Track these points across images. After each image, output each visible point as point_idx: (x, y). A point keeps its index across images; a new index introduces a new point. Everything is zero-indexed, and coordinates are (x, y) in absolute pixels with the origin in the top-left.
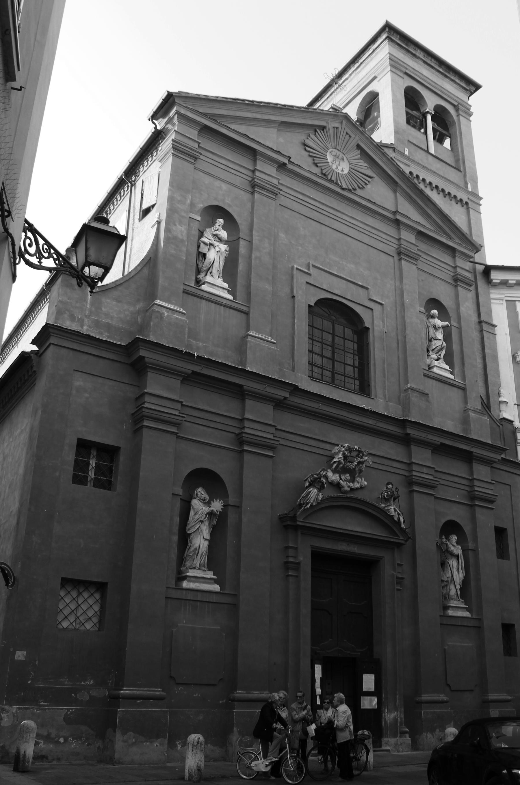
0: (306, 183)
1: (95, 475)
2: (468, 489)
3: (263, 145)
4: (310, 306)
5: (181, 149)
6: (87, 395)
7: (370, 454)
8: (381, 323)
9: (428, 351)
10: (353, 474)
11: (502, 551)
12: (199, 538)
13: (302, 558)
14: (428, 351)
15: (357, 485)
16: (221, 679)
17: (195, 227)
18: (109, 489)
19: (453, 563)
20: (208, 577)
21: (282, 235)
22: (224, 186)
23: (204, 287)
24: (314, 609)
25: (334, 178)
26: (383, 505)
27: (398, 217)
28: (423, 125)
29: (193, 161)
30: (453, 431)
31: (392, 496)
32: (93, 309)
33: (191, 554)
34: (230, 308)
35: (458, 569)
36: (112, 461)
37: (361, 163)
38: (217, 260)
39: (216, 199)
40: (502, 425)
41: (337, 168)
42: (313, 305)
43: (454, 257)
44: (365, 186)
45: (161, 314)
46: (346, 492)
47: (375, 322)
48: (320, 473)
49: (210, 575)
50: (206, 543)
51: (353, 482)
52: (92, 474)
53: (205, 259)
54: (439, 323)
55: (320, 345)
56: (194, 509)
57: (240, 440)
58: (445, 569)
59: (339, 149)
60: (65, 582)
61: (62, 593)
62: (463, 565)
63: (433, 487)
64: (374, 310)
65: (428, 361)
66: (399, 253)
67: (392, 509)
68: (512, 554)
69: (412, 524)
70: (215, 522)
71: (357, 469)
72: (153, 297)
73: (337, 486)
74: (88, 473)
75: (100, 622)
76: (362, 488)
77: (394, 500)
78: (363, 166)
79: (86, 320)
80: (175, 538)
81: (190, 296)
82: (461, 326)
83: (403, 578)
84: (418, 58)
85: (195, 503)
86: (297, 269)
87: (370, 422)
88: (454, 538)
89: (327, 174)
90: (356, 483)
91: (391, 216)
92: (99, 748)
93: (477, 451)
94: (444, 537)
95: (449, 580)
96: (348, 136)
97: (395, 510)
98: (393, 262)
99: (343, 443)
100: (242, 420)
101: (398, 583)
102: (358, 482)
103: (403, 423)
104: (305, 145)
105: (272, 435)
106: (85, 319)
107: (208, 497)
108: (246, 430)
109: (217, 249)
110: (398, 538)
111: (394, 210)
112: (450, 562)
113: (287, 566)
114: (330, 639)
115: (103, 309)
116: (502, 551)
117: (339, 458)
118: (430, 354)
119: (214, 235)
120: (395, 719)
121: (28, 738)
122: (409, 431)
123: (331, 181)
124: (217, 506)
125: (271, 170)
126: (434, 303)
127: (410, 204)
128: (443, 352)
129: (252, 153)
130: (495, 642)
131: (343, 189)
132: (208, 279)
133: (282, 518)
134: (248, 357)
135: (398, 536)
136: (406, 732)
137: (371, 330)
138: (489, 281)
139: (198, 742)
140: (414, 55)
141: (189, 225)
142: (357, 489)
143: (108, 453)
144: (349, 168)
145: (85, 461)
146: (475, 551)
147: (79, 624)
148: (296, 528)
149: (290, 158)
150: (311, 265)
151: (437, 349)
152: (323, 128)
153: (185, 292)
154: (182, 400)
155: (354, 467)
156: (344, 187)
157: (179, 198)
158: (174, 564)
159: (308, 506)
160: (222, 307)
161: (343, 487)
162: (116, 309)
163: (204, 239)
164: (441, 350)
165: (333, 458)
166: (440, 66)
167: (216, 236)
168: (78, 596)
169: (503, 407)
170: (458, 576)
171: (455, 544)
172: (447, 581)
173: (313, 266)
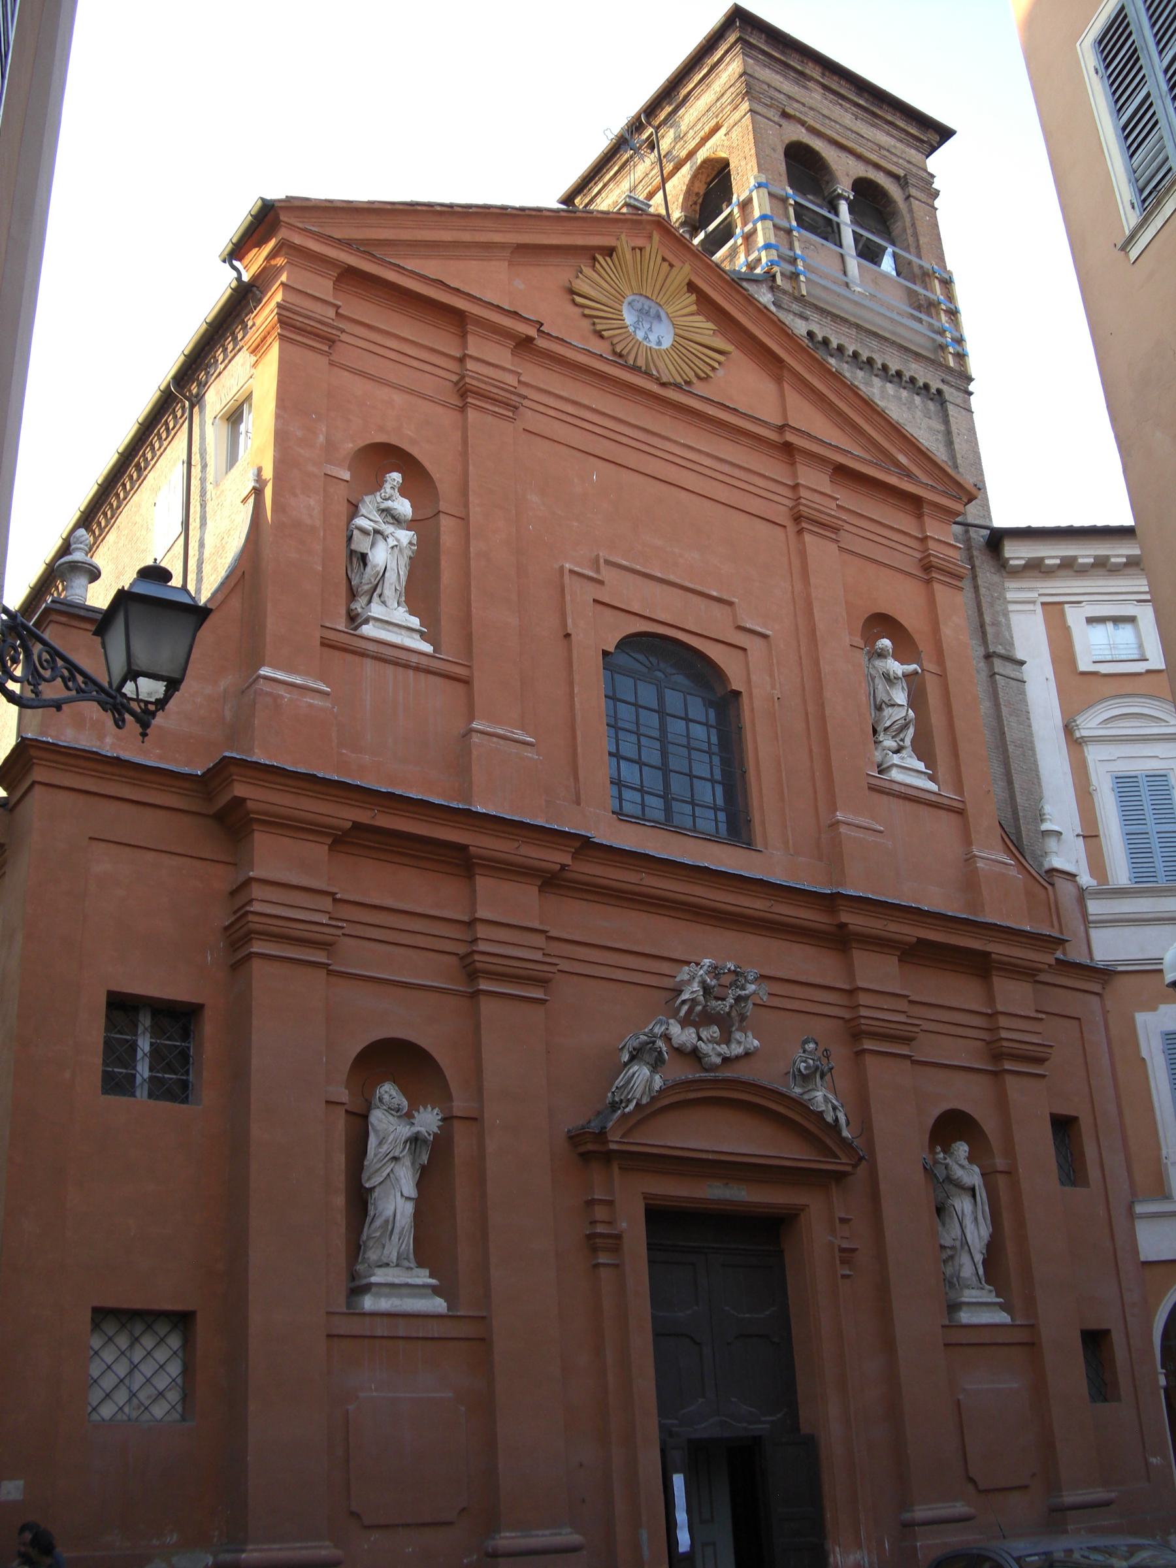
1: (151, 1070)
3: (480, 300)
4: (605, 654)
8: (768, 678)
9: (875, 732)
10: (726, 1025)
11: (1072, 1169)
12: (392, 1197)
13: (624, 1225)
14: (875, 732)
15: (736, 1050)
16: (463, 1509)
17: (340, 494)
18: (185, 1100)
20: (419, 1281)
21: (534, 498)
22: (398, 398)
24: (659, 1334)
25: (641, 362)
26: (798, 1090)
27: (790, 437)
28: (830, 231)
31: (817, 1068)
35: (976, 1219)
36: (186, 1035)
38: (392, 565)
40: (1052, 885)
41: (646, 338)
43: (920, 516)
44: (711, 374)
45: (276, 698)
46: (713, 1068)
49: (422, 1277)
50: (409, 1208)
51: (728, 1042)
52: (143, 1070)
53: (365, 565)
54: (895, 667)
55: (634, 738)
56: (376, 1131)
58: (947, 1220)
61: (96, 1342)
63: (907, 1040)
64: (749, 652)
65: (878, 756)
66: (798, 518)
67: (820, 1097)
68: (1094, 1173)
69: (866, 1127)
70: (425, 1159)
71: (734, 1014)
73: (695, 1055)
74: (134, 1068)
75: (185, 1399)
77: (822, 1076)
78: (704, 328)
80: (340, 1201)
82: (944, 670)
83: (854, 1250)
84: (811, 79)
85: (379, 1119)
86: (571, 571)
88: (962, 1149)
89: (624, 352)
90: (733, 1046)
91: (772, 435)
93: (999, 949)
94: (939, 1149)
95: (958, 1244)
96: (666, 264)
99: (702, 959)
100: (471, 923)
101: (843, 1262)
102: (739, 1043)
103: (831, 901)
104: (572, 292)
105: (541, 953)
109: (391, 542)
110: (835, 1160)
114: (701, 1400)
116: (1072, 1169)
119: (383, 510)
122: (845, 918)
123: (635, 369)
124: (428, 1121)
125: (501, 354)
130: (1068, 1371)
131: (663, 385)
132: (376, 610)
133: (575, 1138)
135: (837, 1157)
137: (745, 699)
138: (1001, 564)
140: (802, 74)
142: (738, 1058)
143: (178, 1018)
144: (672, 335)
145: (127, 1041)
146: (1010, 1173)
148: (608, 1157)
150: (602, 561)
151: (895, 727)
152: (610, 251)
153: (326, 644)
155: (727, 1009)
156: (664, 380)
157: (299, 434)
160: (411, 673)
163: (360, 522)
164: (905, 727)
165: (681, 991)
166: (860, 95)
168: (131, 1346)
169: (1052, 844)
170: (977, 1234)
171: (965, 1163)
172: (953, 1248)
173: (607, 562)
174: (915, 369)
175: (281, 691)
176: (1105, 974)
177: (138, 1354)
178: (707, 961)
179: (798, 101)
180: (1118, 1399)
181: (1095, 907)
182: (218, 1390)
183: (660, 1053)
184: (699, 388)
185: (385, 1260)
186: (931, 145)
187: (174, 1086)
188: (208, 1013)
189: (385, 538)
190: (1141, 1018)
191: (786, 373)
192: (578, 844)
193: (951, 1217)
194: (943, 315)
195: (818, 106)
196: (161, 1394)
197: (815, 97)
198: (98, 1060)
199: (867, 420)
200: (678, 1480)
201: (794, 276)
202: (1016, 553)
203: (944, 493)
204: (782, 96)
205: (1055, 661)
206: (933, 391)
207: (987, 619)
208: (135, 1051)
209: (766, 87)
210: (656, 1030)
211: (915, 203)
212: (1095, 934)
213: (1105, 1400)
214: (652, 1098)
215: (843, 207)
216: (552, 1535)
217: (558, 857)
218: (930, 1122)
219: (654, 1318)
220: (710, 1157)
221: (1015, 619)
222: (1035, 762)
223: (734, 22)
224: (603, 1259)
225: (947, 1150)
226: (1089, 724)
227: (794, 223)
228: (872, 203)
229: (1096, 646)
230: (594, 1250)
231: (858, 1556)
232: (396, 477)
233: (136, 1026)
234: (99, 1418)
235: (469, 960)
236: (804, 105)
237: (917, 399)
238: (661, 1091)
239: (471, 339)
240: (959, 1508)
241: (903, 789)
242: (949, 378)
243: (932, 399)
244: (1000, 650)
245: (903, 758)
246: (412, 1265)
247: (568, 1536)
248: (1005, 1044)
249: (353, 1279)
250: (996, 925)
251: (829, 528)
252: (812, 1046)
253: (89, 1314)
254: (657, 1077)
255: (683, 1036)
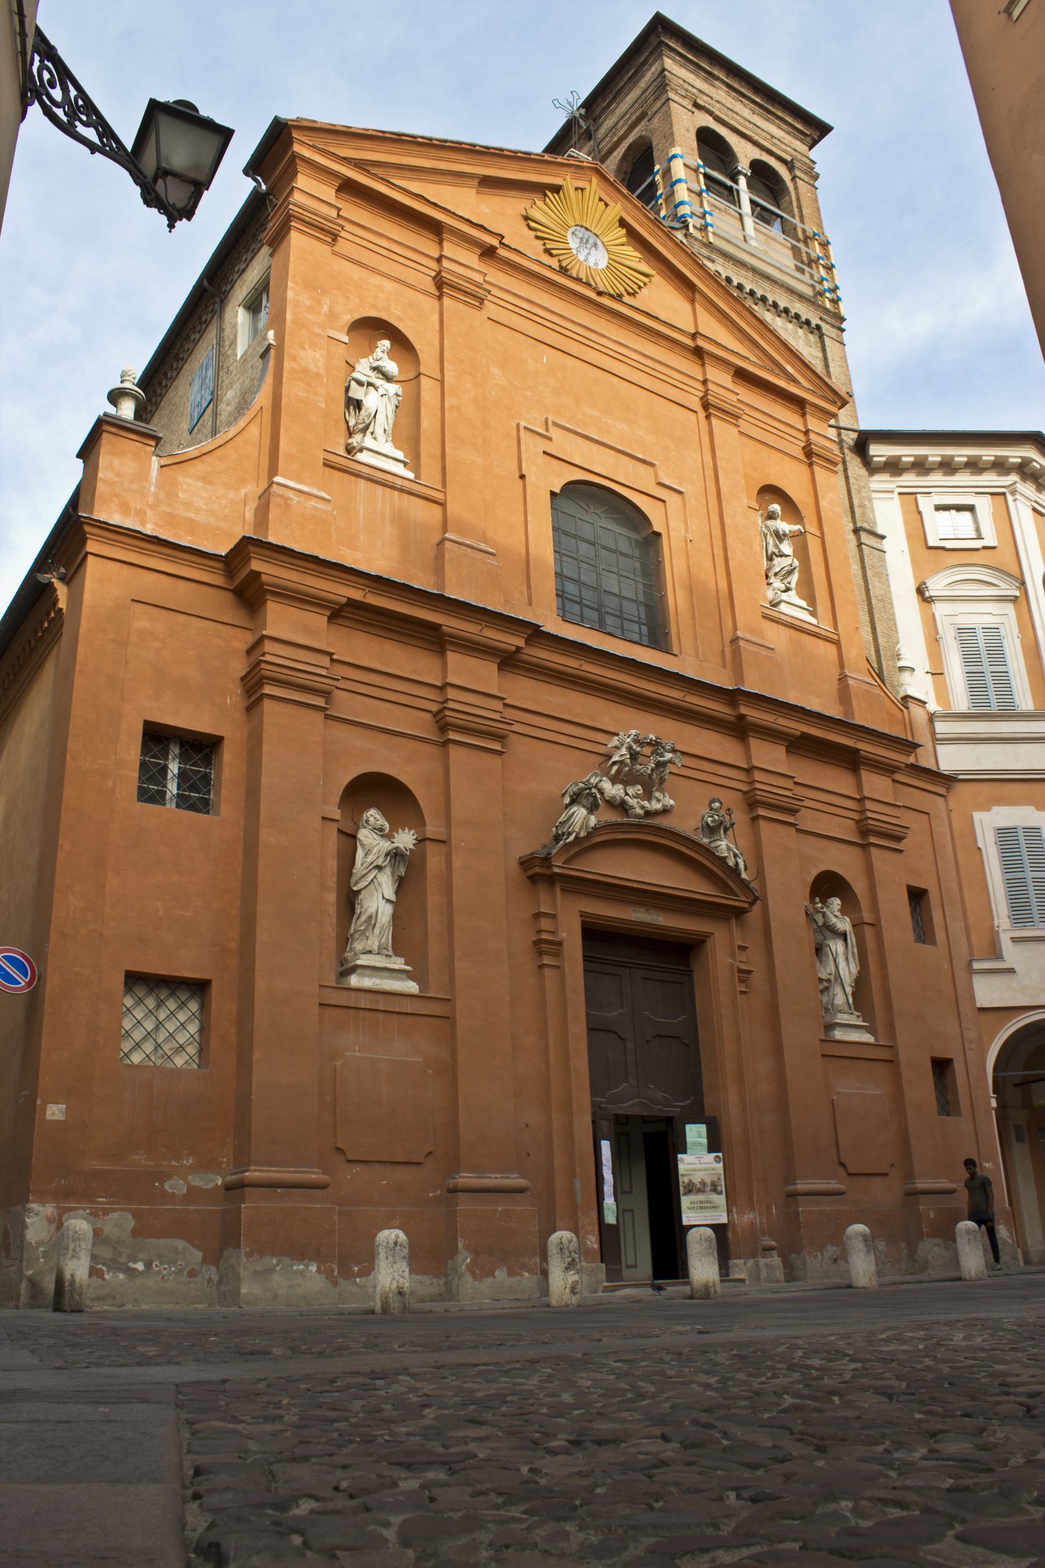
0: (533, 281)
2: (856, 816)
3: (454, 213)
4: (553, 494)
5: (307, 219)
6: (158, 645)
7: (674, 751)
8: (682, 525)
9: (767, 577)
11: (924, 931)
12: (375, 898)
13: (565, 934)
14: (767, 577)
15: (656, 806)
16: (430, 1153)
17: (340, 352)
19: (837, 946)
20: (397, 967)
21: (496, 371)
22: (388, 285)
23: (361, 457)
24: (592, 1029)
25: (582, 276)
27: (701, 343)
28: (731, 195)
29: (330, 240)
30: (820, 711)
31: (721, 823)
32: (162, 495)
33: (363, 928)
34: (410, 493)
35: (847, 959)
36: (208, 762)
37: (629, 250)
39: (374, 307)
40: (907, 708)
41: (586, 260)
42: (558, 491)
43: (803, 415)
45: (286, 500)
46: (637, 816)
47: (671, 523)
48: (588, 780)
49: (398, 963)
51: (649, 800)
52: (172, 787)
53: (360, 409)
54: (783, 526)
56: (363, 845)
57: (443, 727)
58: (824, 959)
59: (588, 227)
60: (135, 980)
61: (129, 1002)
62: (855, 950)
63: (793, 812)
65: (770, 594)
66: (706, 405)
67: (723, 845)
68: (940, 935)
69: (760, 874)
70: (402, 871)
71: (654, 776)
72: (273, 470)
73: (622, 807)
74: (165, 786)
75: (202, 1030)
76: (665, 811)
77: (726, 830)
78: (632, 256)
79: (150, 513)
80: (332, 897)
81: (336, 472)
82: (822, 533)
83: (749, 972)
84: (717, 78)
85: (365, 835)
86: (526, 428)
87: (673, 694)
88: (836, 903)
90: (654, 802)
91: (688, 342)
92: (210, 1280)
93: (866, 748)
94: (817, 900)
95: (832, 978)
96: (602, 203)
97: (729, 849)
98: (695, 421)
99: (628, 729)
100: (442, 688)
101: (741, 981)
102: (659, 800)
103: (733, 696)
104: (527, 218)
106: (148, 511)
107: (387, 826)
108: (451, 705)
109: (381, 391)
110: (733, 898)
111: (693, 331)
112: (832, 944)
113: (540, 947)
114: (625, 1084)
115: (180, 495)
116: (924, 931)
117: (622, 755)
118: (771, 581)
120: (752, 1224)
121: (78, 1249)
122: (744, 710)
123: (578, 280)
125: (471, 258)
126: (771, 491)
127: (720, 322)
128: (795, 578)
129: (434, 228)
130: (921, 1087)
131: (600, 294)
132: (368, 442)
133: (525, 863)
134: (447, 576)
135: (734, 894)
136: (772, 1249)
139: (396, 1243)
141: (328, 349)
143: (201, 748)
145: (159, 764)
146: (876, 925)
147: (163, 1057)
148: (552, 879)
149: (503, 237)
152: (557, 189)
153: (327, 464)
154: (332, 651)
155: (649, 772)
156: (601, 288)
157: (308, 303)
158: (332, 943)
159: (572, 838)
160: (396, 493)
161: (632, 807)
162: (204, 494)
164: (790, 572)
165: (610, 757)
167: (376, 369)
170: (848, 970)
171: (838, 914)
172: (828, 981)
173: (555, 424)
174: (798, 307)
175: (291, 494)
176: (949, 780)
177: (162, 1016)
178: (633, 732)
179: (707, 95)
180: (959, 1115)
181: (940, 727)
182: (230, 1047)
183: (595, 797)
184: (627, 299)
185: (368, 949)
186: (813, 139)
187: (197, 795)
188: (227, 745)
189: (376, 388)
190: (977, 816)
191: (697, 296)
192: (530, 632)
193: (827, 956)
194: (821, 268)
195: (723, 101)
196: (182, 1048)
197: (720, 94)
198: (135, 775)
199: (762, 336)
200: (606, 1146)
201: (704, 228)
202: (879, 452)
203: (824, 398)
204: (694, 91)
205: (910, 538)
206: (813, 325)
207: (856, 502)
208: (166, 773)
209: (681, 82)
210: (592, 781)
211: (799, 182)
212: (940, 749)
213: (948, 1115)
214: (589, 833)
215: (742, 181)
216: (502, 1178)
217: (513, 641)
218: (811, 879)
219: (588, 1015)
220: (635, 885)
221: (876, 504)
222: (893, 614)
223: (656, 27)
224: (547, 960)
225: (824, 902)
226: (936, 586)
227: (704, 187)
228: (764, 177)
229: (944, 528)
230: (540, 953)
231: (751, 1216)
232: (386, 343)
233: (168, 754)
234: (129, 1062)
235: (441, 715)
236: (712, 98)
237: (800, 331)
238: (595, 828)
239: (445, 244)
240: (833, 1185)
241: (789, 620)
242: (825, 317)
243: (812, 333)
244: (865, 525)
245: (789, 596)
246: (390, 953)
247: (515, 1180)
248: (871, 822)
249: (342, 965)
250: (863, 727)
251: (732, 416)
252: (717, 804)
253: (121, 978)
254: (592, 818)
255: (613, 790)
